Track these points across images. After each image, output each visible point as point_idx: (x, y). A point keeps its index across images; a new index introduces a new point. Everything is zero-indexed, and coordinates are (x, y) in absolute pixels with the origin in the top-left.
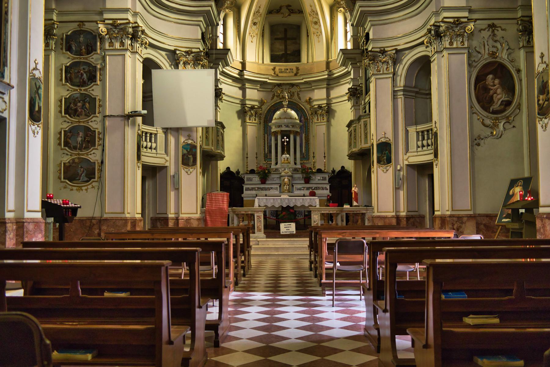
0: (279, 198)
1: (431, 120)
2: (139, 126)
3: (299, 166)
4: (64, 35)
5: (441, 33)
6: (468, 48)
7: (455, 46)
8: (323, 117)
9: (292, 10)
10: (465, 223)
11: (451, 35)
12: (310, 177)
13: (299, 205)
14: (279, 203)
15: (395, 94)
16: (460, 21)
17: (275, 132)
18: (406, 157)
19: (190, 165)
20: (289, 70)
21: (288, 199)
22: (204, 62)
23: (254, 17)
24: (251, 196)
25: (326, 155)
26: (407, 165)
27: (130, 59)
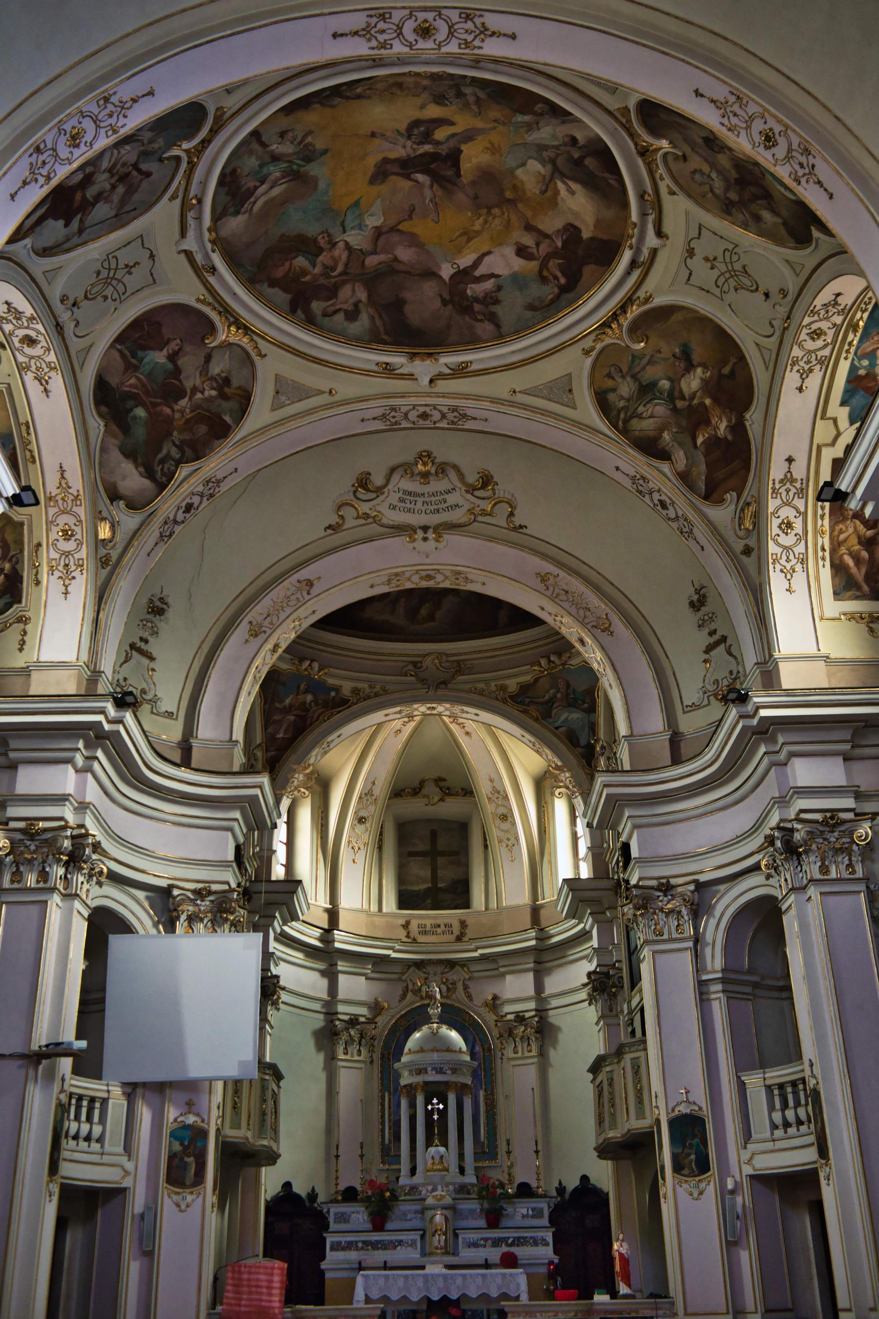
0: (419, 1275)
1: (799, 1056)
2: (63, 1080)
3: (470, 1178)
5: (798, 844)
6: (866, 879)
7: (833, 875)
8: (529, 1045)
9: (448, 789)
11: (822, 850)
13: (473, 1293)
15: (704, 989)
16: (838, 818)
17: (410, 1085)
18: (745, 1155)
20: (442, 927)
21: (445, 1277)
22: (237, 914)
23: (361, 806)
24: (347, 1266)
25: (540, 1148)
26: (752, 1177)
27: (59, 911)
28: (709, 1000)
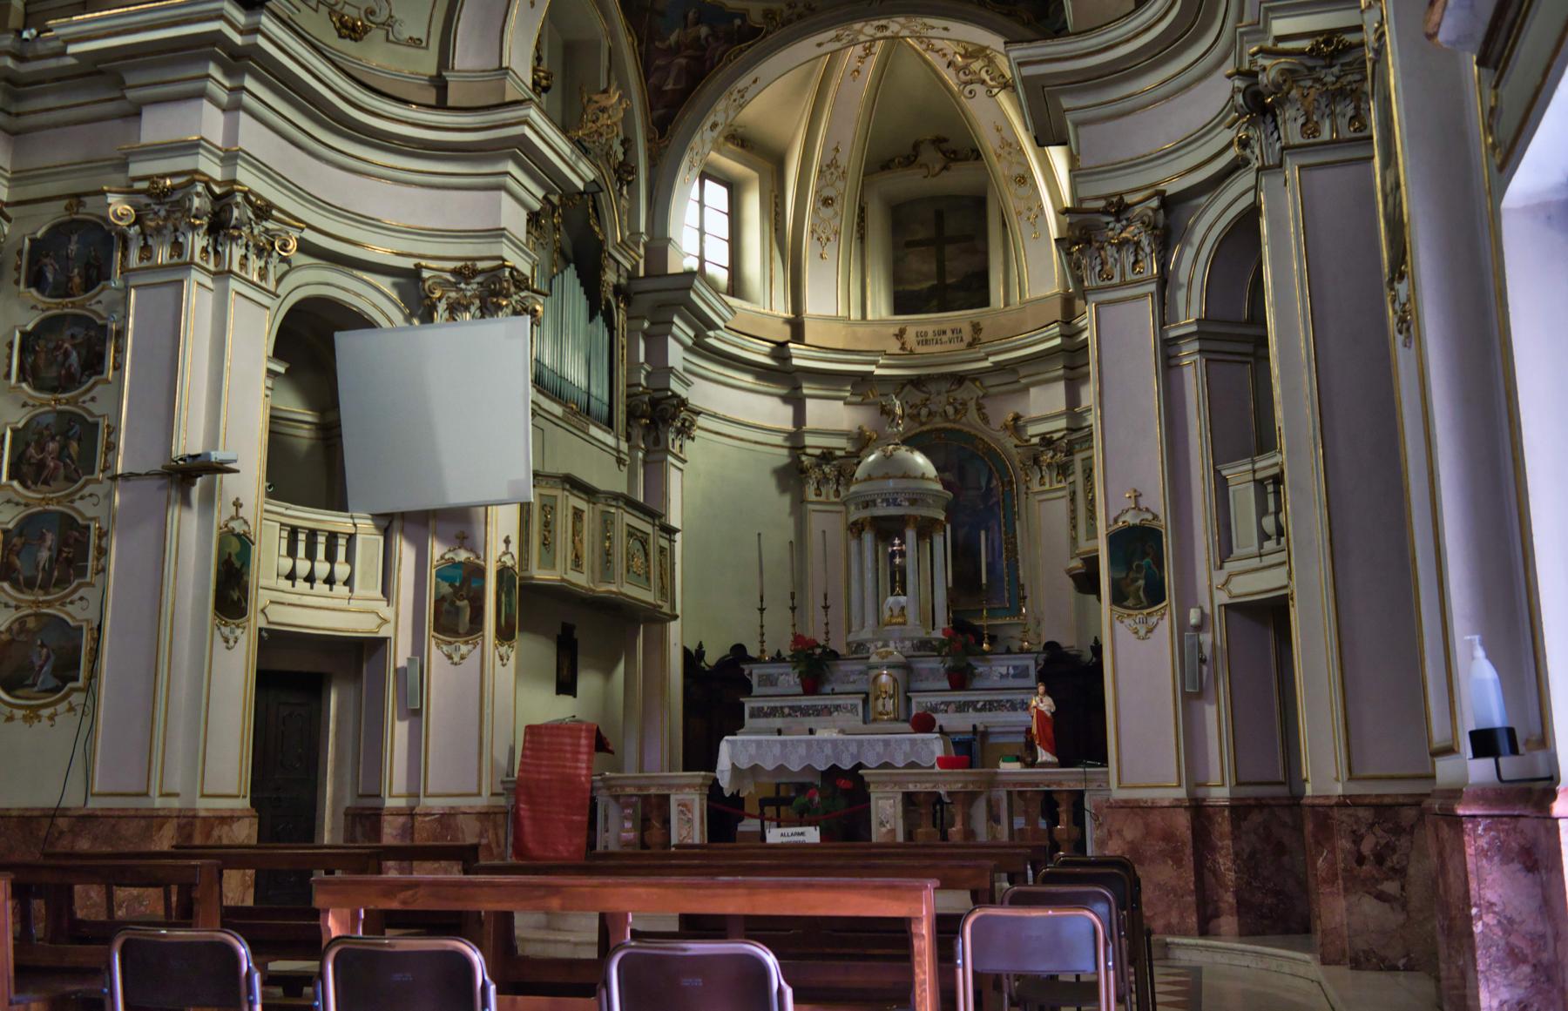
4: (27, 241)
7: (1326, 134)
9: (954, 152)
10: (1412, 833)
12: (969, 665)
14: (878, 754)
15: (1172, 351)
16: (1339, 42)
18: (1220, 578)
19: (461, 631)
20: (949, 334)
23: (823, 182)
26: (1227, 606)
28: (1178, 366)
